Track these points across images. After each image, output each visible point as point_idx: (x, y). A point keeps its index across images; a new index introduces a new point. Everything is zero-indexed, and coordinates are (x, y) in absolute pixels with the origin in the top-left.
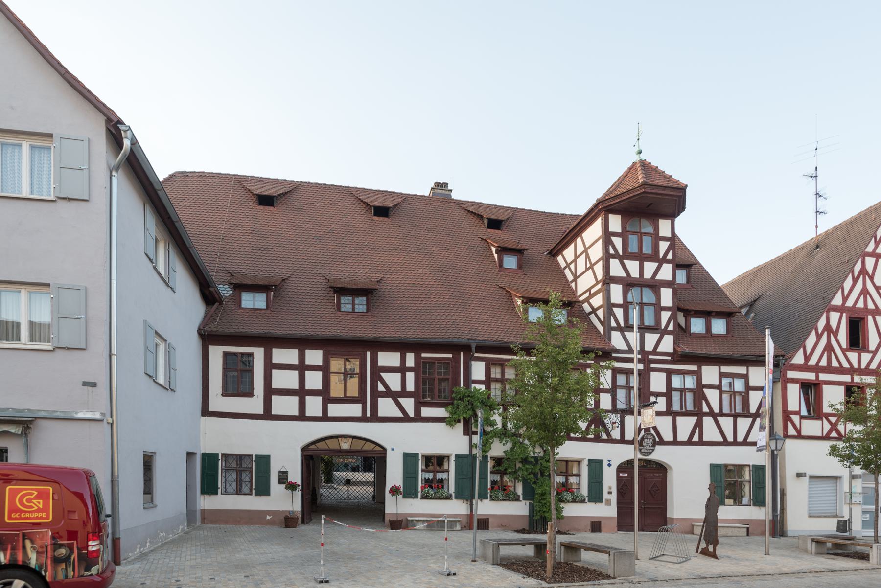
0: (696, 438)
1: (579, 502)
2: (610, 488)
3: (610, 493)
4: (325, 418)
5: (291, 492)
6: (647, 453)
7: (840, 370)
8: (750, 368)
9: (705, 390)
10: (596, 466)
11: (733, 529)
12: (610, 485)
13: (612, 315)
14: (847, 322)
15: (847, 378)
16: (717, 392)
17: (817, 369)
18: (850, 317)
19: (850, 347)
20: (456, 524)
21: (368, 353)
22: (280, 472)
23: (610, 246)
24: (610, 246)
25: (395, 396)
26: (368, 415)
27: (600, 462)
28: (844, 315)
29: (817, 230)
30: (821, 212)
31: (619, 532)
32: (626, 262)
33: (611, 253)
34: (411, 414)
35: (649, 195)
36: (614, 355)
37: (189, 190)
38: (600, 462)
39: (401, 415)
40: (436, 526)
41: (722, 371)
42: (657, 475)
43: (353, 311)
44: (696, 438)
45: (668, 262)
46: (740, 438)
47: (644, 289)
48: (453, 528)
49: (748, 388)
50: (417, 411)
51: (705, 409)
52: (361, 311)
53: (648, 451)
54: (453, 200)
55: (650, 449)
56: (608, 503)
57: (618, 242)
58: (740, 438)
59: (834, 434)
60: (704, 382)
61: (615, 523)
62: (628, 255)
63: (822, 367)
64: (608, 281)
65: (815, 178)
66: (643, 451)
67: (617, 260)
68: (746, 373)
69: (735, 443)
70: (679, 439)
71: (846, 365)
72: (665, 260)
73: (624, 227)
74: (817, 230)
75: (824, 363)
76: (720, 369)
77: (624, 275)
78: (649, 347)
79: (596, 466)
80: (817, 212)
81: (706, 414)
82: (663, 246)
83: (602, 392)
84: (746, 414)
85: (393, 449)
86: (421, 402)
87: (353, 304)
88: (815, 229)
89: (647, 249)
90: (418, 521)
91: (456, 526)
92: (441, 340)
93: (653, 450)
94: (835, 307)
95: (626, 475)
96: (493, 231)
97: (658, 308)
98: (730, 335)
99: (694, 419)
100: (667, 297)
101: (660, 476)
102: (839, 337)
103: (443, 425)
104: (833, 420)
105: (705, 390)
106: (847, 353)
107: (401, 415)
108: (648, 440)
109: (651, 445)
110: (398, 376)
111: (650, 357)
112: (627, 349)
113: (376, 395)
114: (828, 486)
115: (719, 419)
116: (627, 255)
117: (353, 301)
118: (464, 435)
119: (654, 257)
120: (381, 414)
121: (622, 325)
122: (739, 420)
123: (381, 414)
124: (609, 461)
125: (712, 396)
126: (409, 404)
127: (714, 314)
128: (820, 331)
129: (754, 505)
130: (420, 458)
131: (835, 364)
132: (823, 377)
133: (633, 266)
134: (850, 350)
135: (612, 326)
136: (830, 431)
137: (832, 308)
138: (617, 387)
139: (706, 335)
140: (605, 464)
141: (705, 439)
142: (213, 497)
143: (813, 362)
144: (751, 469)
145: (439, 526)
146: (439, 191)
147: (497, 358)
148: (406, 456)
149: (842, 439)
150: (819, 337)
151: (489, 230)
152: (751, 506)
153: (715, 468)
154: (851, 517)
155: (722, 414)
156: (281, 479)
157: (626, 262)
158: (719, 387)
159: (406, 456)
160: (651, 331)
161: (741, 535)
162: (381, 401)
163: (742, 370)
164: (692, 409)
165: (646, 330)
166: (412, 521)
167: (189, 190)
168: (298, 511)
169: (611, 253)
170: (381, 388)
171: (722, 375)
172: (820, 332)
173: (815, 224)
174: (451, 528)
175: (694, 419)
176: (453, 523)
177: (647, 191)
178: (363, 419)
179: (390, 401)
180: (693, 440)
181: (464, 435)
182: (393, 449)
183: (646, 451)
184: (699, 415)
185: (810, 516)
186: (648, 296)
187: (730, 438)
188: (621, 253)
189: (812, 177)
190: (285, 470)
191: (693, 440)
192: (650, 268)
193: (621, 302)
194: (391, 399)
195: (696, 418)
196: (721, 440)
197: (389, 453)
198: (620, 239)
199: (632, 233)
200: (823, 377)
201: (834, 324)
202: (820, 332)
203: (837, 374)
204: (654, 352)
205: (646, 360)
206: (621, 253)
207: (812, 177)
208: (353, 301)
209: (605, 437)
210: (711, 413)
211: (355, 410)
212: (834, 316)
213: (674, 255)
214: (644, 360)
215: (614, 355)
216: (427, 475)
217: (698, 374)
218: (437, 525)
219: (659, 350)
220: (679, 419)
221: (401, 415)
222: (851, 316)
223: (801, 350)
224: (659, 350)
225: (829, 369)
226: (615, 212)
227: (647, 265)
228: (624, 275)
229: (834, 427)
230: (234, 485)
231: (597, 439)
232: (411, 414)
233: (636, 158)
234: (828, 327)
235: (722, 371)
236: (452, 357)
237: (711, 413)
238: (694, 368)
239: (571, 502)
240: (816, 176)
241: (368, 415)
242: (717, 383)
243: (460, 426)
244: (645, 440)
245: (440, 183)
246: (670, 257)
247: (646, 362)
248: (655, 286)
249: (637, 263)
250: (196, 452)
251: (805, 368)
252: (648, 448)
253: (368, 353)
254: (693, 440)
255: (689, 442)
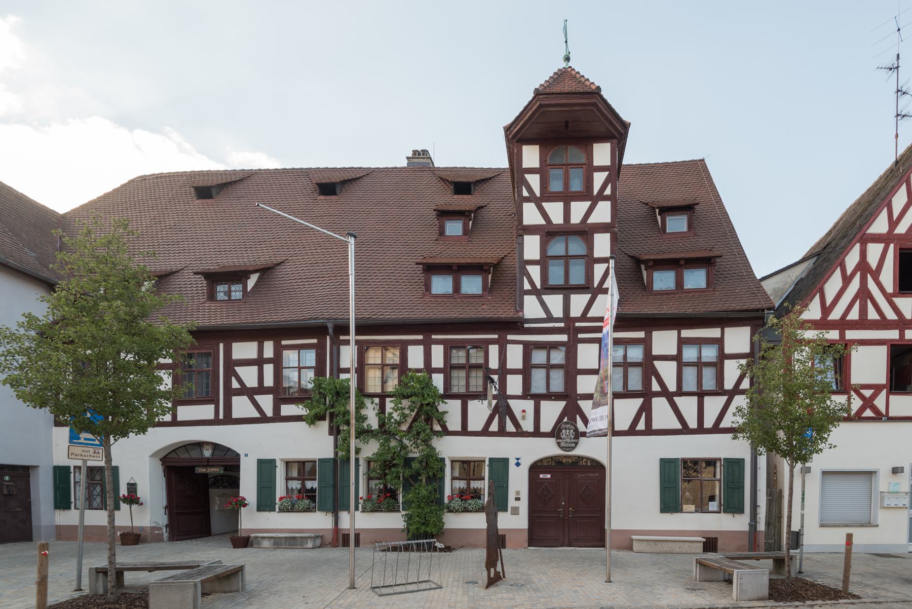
0: (641, 426)
1: (474, 512)
2: (518, 493)
3: (518, 499)
4: (175, 423)
5: (129, 506)
6: (568, 447)
7: (883, 324)
8: (727, 330)
9: (656, 363)
10: (500, 466)
11: (682, 543)
12: (518, 489)
13: (525, 275)
14: (895, 256)
15: (893, 334)
16: (674, 364)
17: (843, 324)
18: (900, 249)
19: (900, 290)
20: (307, 541)
21: (221, 346)
22: (128, 484)
23: (523, 187)
24: (523, 187)
25: (251, 393)
26: (221, 417)
27: (505, 461)
28: (892, 246)
29: (897, 140)
30: (904, 116)
31: (529, 548)
32: (546, 205)
33: (524, 195)
34: (269, 413)
35: (550, 109)
36: (526, 325)
37: (396, 222)
38: (505, 461)
39: (258, 416)
40: (283, 543)
41: (682, 336)
42: (592, 475)
43: (230, 299)
44: (641, 426)
45: (606, 198)
46: (708, 423)
47: (570, 238)
48: (304, 546)
49: (723, 356)
50: (276, 409)
51: (656, 387)
52: (238, 298)
53: (570, 445)
54: (887, 232)
55: (572, 443)
56: (515, 511)
57: (534, 181)
58: (708, 423)
59: (868, 413)
60: (655, 352)
61: (525, 536)
62: (549, 195)
63: (852, 321)
64: (521, 232)
65: (896, 70)
66: (562, 444)
67: (533, 204)
68: (719, 336)
69: (701, 429)
70: (471, 428)
71: (891, 315)
72: (601, 197)
73: (542, 160)
74: (897, 140)
75: (854, 315)
76: (679, 334)
77: (543, 222)
78: (576, 310)
79: (500, 466)
80: (898, 115)
81: (657, 394)
82: (599, 179)
83: (266, 363)
84: (719, 391)
85: (246, 455)
86: (281, 399)
87: (230, 291)
88: (895, 139)
89: (576, 185)
90: (263, 538)
91: (307, 544)
92: (296, 322)
93: (576, 444)
94: (877, 237)
95: (549, 476)
96: (460, 196)
97: (590, 260)
98: (711, 289)
99: (639, 402)
100: (602, 245)
101: (596, 476)
102: (882, 278)
103: (302, 425)
104: (867, 393)
105: (656, 363)
106: (896, 300)
107: (257, 415)
108: (568, 431)
109: (573, 437)
110: (254, 369)
111: (577, 324)
112: (546, 317)
113: (230, 393)
114: (857, 486)
115: (677, 400)
116: (547, 196)
117: (230, 288)
118: (330, 435)
119: (586, 194)
120: (235, 415)
121: (539, 287)
122: (707, 400)
123: (235, 415)
124: (518, 459)
125: (667, 371)
126: (266, 402)
127: (682, 262)
128: (849, 272)
129: (725, 511)
130: (278, 463)
131: (872, 315)
132: (851, 335)
133: (555, 210)
134: (900, 295)
135: (869, 318)
136: (862, 409)
137: (872, 239)
138: (384, 363)
139: (676, 291)
140: (512, 463)
141: (655, 426)
142: (67, 512)
143: (836, 315)
144: (722, 464)
145: (287, 544)
146: (415, 160)
147: (373, 340)
148: (261, 463)
149: (882, 419)
150: (847, 280)
151: (456, 196)
152: (720, 512)
153: (666, 465)
154: (802, 527)
155: (680, 393)
156: (130, 492)
157: (546, 205)
158: (678, 358)
159: (261, 463)
160: (579, 291)
161: (693, 551)
162: (236, 400)
163: (715, 333)
164: (622, 391)
165: (572, 291)
166: (256, 537)
167: (396, 222)
168: (148, 527)
169: (524, 195)
170: (235, 385)
171: (682, 342)
172: (849, 272)
173: (895, 133)
174: (301, 545)
175: (639, 402)
176: (304, 539)
177: (543, 103)
178: (215, 422)
179: (245, 399)
180: (720, 427)
181: (330, 435)
182: (246, 455)
183: (567, 445)
184: (647, 395)
185: (822, 526)
186: (576, 247)
187: (693, 424)
188: (538, 195)
189: (891, 69)
190: (134, 482)
191: (638, 428)
192: (578, 209)
193: (537, 257)
194: (246, 396)
195: (642, 399)
196: (678, 426)
197: (242, 458)
198: (537, 177)
199: (554, 166)
200: (851, 335)
201: (873, 261)
202: (849, 273)
203: (877, 329)
204: (584, 317)
205: (572, 329)
206: (538, 194)
207: (891, 69)
208: (230, 288)
209: (510, 427)
210: (664, 392)
211: (206, 411)
212: (874, 251)
213: (614, 190)
214: (569, 329)
215: (526, 325)
216: (294, 484)
217: (646, 343)
218: (285, 542)
219: (590, 315)
220: (544, 404)
221: (258, 416)
222: (904, 247)
223: (817, 298)
224: (590, 315)
225: (863, 323)
226: (530, 142)
227: (574, 205)
228: (543, 222)
229: (868, 403)
230: (98, 499)
231: (502, 432)
232: (269, 413)
233: (562, 65)
234: (863, 266)
235: (682, 336)
236: (282, 342)
237: (664, 392)
238: (641, 335)
239: (462, 511)
240: (897, 68)
241: (221, 417)
242: (674, 352)
243: (325, 425)
244: (564, 431)
245: (417, 151)
246: (608, 192)
247: (572, 332)
248: (585, 232)
249: (560, 205)
250: (37, 465)
251: (823, 324)
252: (568, 440)
253: (221, 346)
254: (638, 428)
255: (632, 431)
